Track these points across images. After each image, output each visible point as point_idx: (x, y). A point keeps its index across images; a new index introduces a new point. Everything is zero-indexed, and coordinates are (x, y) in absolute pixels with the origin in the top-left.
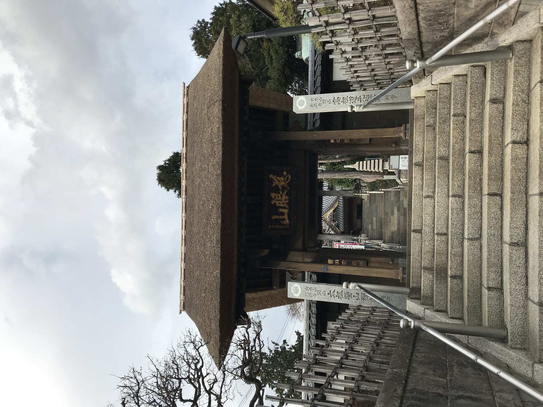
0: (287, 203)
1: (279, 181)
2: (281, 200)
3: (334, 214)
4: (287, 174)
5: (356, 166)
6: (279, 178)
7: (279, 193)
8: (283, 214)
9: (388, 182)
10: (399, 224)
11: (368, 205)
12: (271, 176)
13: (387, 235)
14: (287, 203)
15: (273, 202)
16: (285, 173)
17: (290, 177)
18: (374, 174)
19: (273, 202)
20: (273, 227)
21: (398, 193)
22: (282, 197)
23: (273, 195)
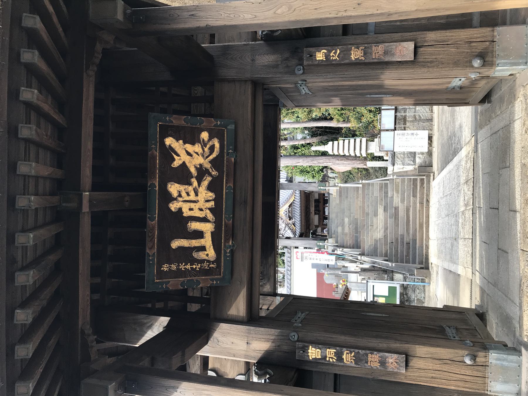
0: (210, 209)
1: (189, 154)
2: (193, 201)
3: (290, 209)
4: (210, 138)
5: (328, 148)
6: (189, 147)
7: (190, 184)
8: (199, 235)
9: (371, 171)
10: (386, 229)
11: (338, 202)
12: (169, 141)
13: (367, 243)
14: (210, 209)
15: (174, 206)
16: (205, 135)
17: (217, 145)
18: (348, 159)
19: (174, 206)
20: (174, 267)
21: (384, 187)
22: (197, 195)
23: (174, 188)
